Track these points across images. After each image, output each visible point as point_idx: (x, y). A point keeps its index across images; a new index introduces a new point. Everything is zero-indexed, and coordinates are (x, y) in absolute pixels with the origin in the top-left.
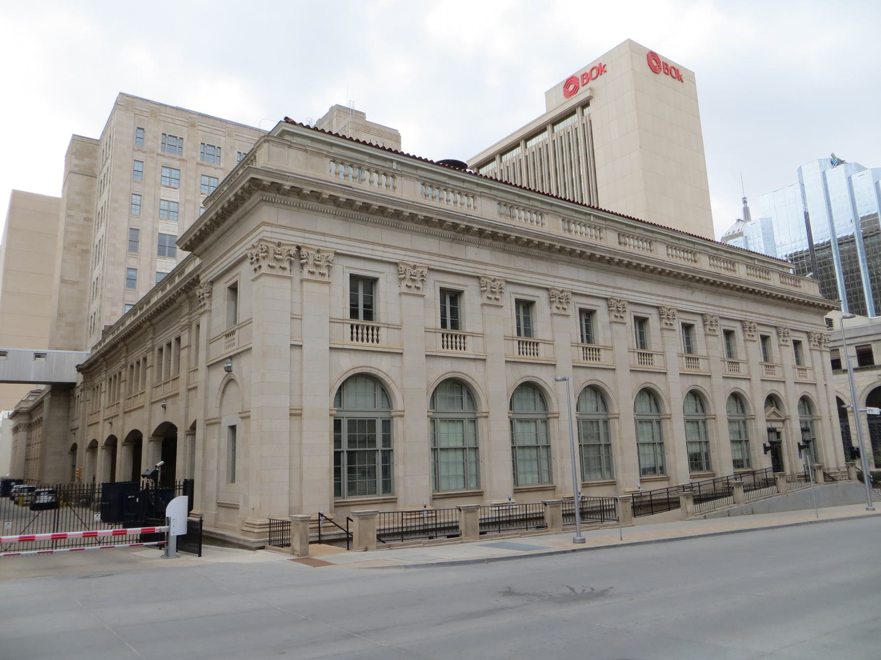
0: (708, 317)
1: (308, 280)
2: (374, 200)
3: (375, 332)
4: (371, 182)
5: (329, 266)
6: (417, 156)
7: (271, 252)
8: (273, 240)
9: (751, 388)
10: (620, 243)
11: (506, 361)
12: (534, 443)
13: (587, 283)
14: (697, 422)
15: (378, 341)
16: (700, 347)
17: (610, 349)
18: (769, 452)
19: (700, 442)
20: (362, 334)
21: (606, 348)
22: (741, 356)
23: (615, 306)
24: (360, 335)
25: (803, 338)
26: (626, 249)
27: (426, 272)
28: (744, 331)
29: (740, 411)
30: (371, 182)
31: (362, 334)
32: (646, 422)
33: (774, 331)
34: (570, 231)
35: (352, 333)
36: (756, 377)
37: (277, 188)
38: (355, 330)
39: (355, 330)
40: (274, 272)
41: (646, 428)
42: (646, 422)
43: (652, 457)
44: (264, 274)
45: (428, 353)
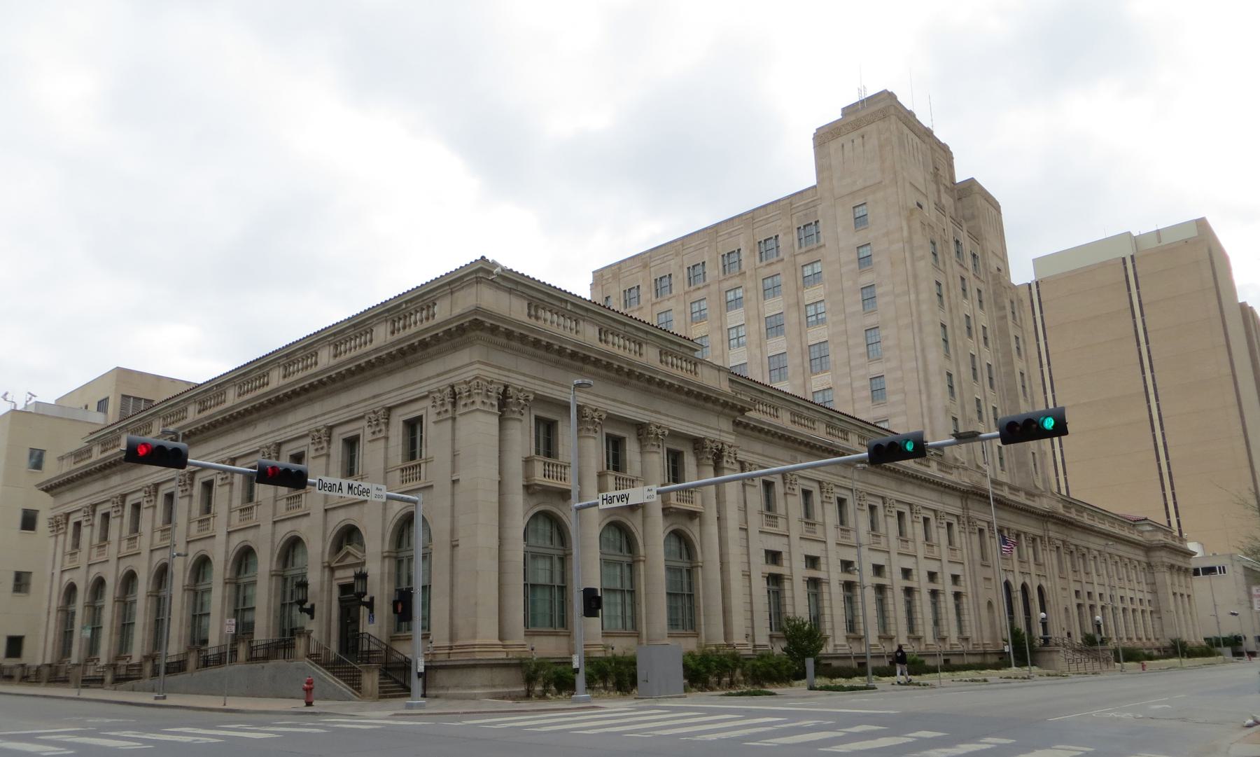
0: (588, 411)
9: (859, 555)
10: (530, 315)
12: (548, 582)
14: (551, 558)
16: (934, 535)
18: (366, 599)
19: (622, 591)
22: (818, 517)
23: (641, 429)
25: (878, 503)
26: (609, 348)
28: (822, 492)
29: (685, 556)
32: (544, 556)
33: (849, 493)
34: (537, 318)
36: (921, 555)
40: (486, 409)
41: (543, 565)
42: (544, 556)
43: (619, 609)
44: (477, 410)
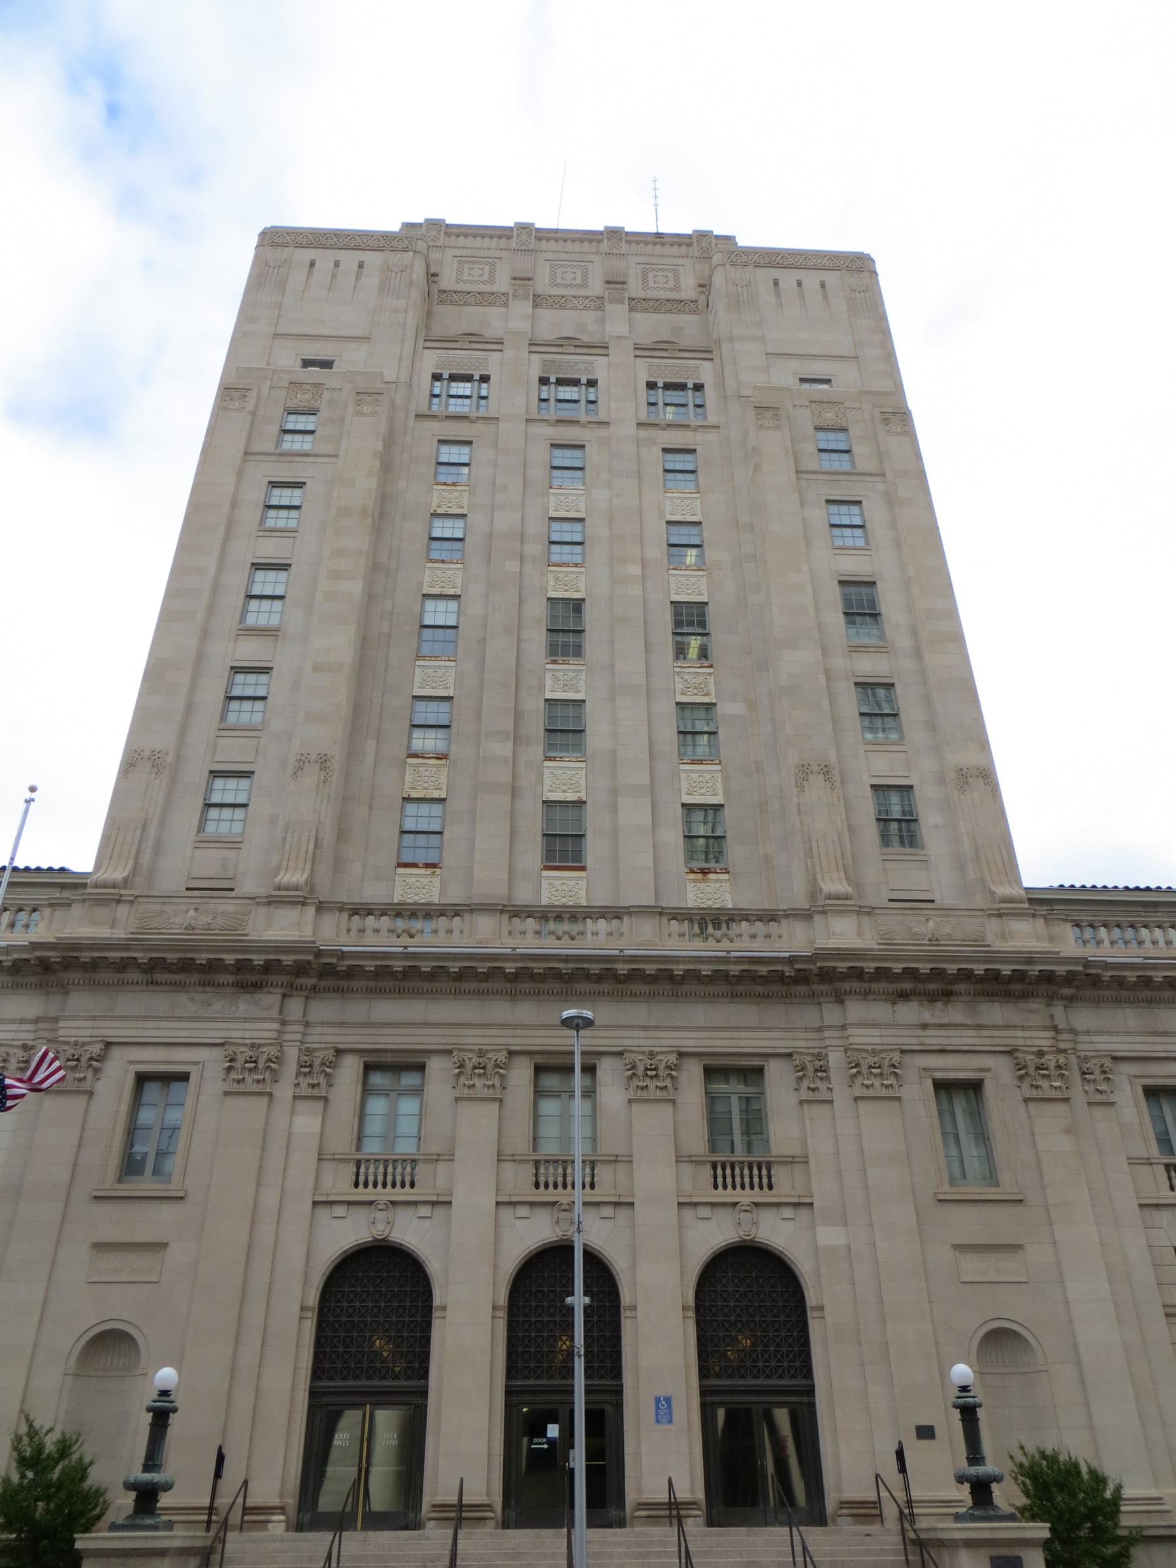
1: (809, 1102)
2: (921, 961)
3: (764, 1172)
4: (1155, 943)
5: (1108, 1079)
6: (1142, 886)
7: (810, 1068)
8: (642, 1049)
11: (1141, 1206)
13: (644, 1028)
15: (770, 1187)
17: (799, 1161)
20: (742, 1177)
21: (790, 1161)
24: (738, 1180)
27: (1108, 1063)
30: (1155, 943)
31: (742, 1177)
35: (715, 1177)
37: (858, 974)
38: (719, 1171)
39: (719, 1171)
45: (1144, 1202)
